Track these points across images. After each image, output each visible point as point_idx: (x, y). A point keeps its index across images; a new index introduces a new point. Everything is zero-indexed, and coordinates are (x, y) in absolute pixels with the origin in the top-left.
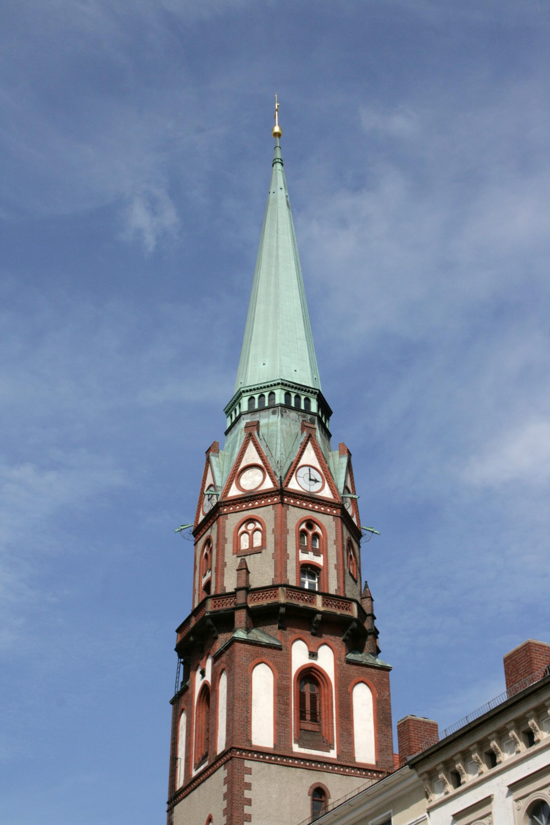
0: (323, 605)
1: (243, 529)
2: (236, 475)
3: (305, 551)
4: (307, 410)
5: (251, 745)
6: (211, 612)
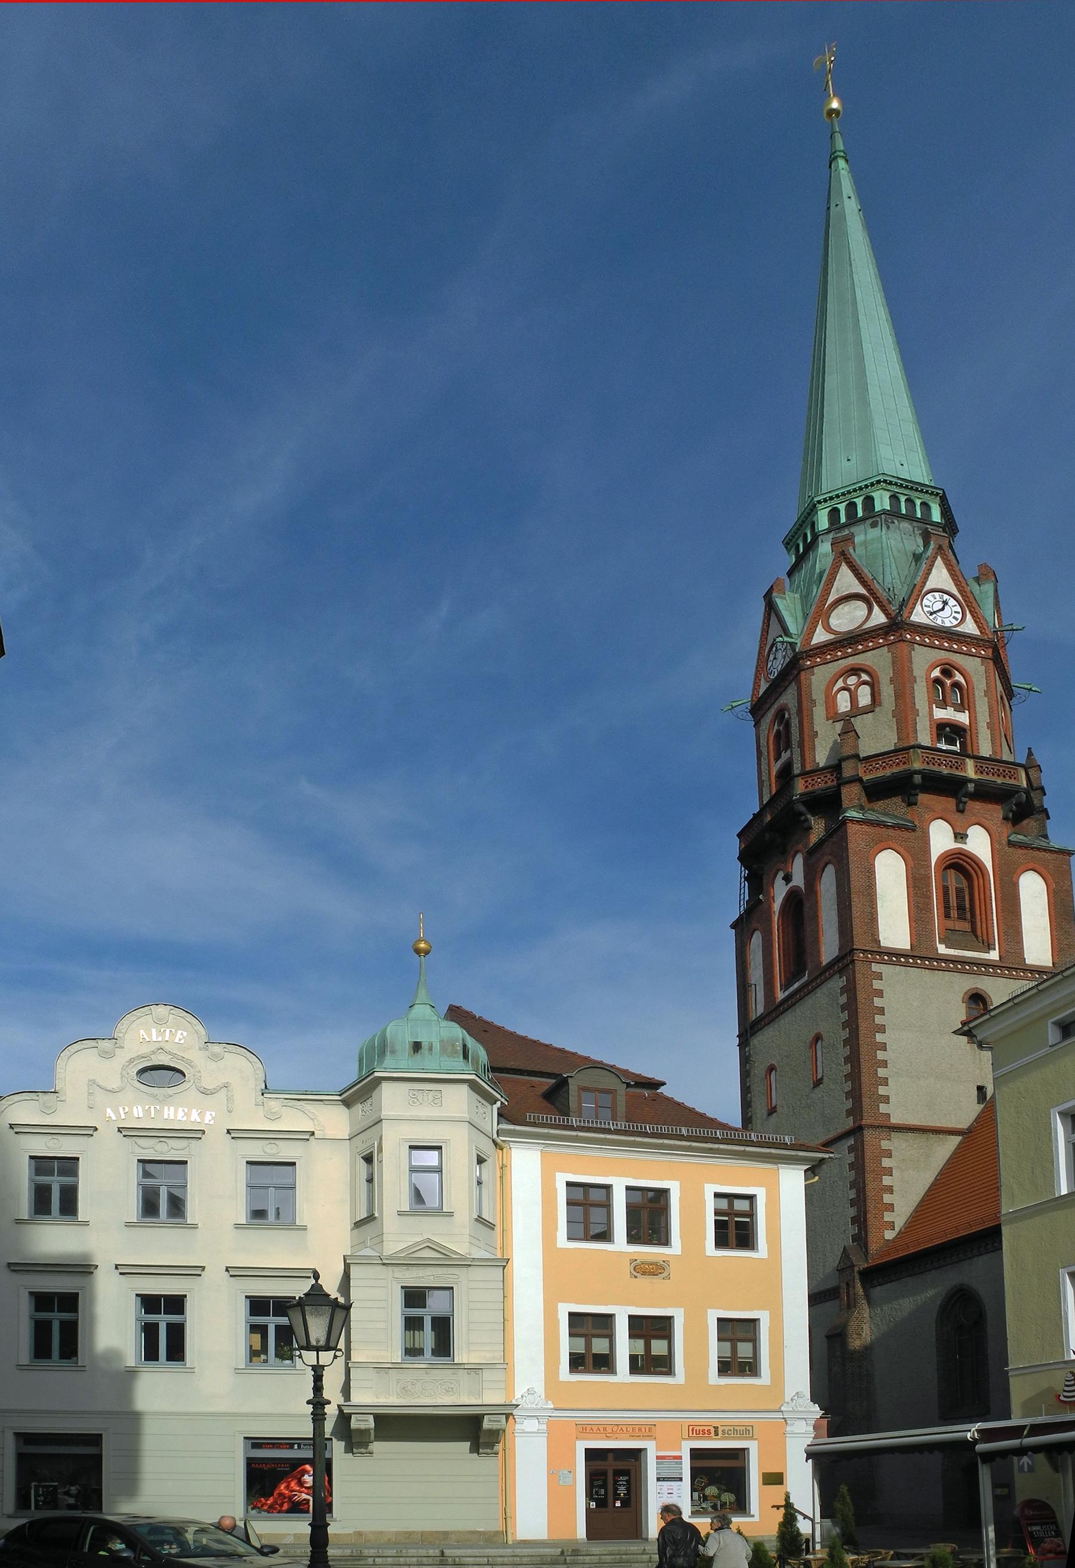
0: (976, 772)
1: (840, 684)
2: (820, 613)
3: (943, 704)
4: (926, 519)
5: (880, 947)
6: (801, 795)
